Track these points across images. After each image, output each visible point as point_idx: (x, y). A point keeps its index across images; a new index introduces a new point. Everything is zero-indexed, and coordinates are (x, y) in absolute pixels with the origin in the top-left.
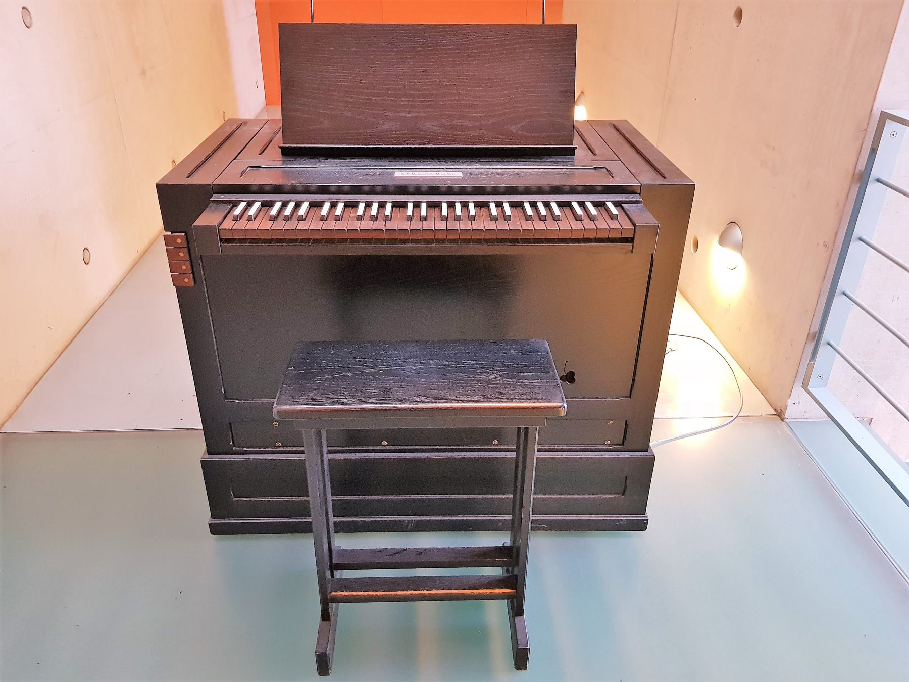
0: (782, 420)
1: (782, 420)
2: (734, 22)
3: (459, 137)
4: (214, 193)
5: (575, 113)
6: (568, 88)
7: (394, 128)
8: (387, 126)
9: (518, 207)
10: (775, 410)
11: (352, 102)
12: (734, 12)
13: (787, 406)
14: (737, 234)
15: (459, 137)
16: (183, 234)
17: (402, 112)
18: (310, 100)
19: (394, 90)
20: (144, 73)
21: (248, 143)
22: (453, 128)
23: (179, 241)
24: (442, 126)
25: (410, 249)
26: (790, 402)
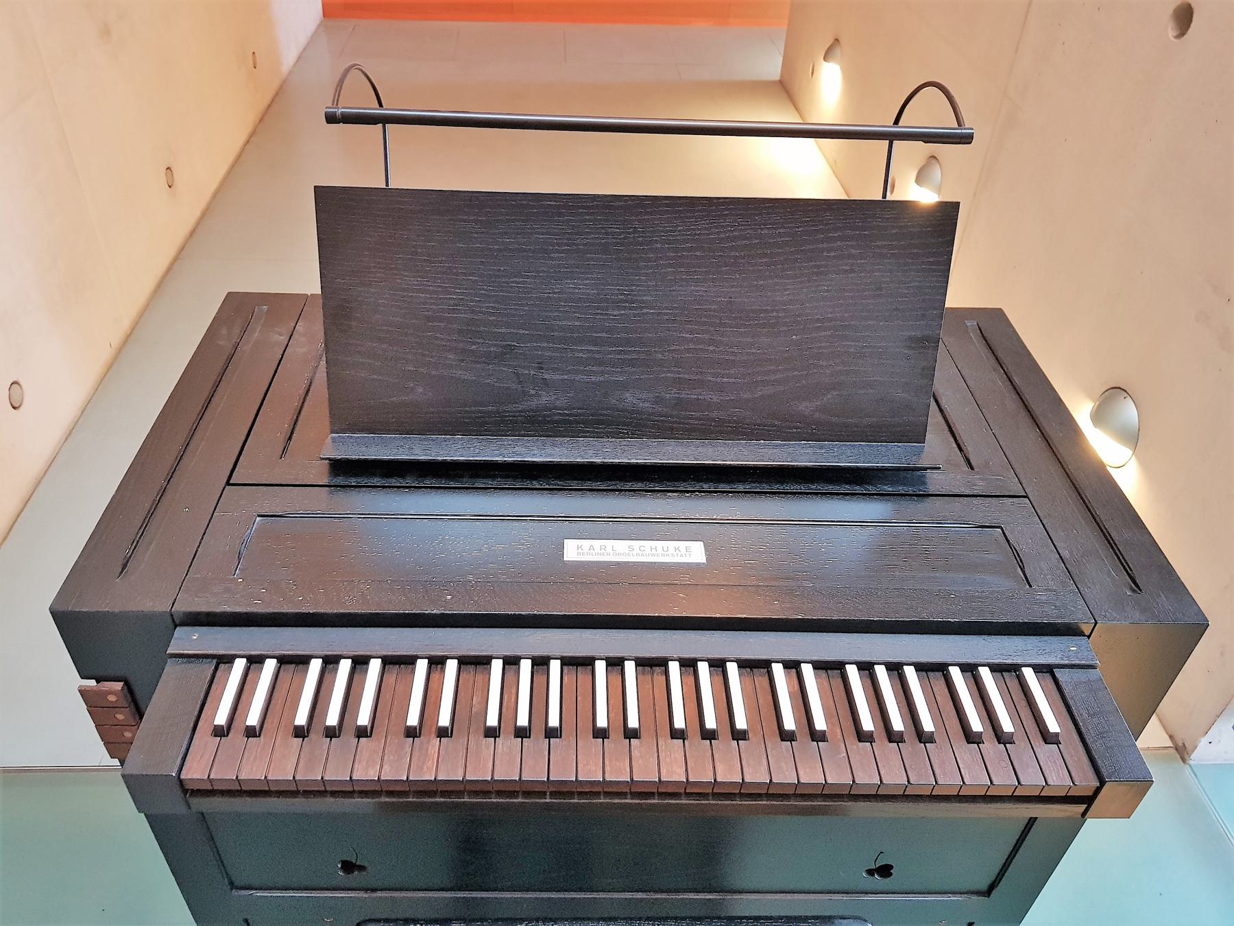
0: (1184, 760)
1: (1184, 760)
2: (1170, 29)
3: (691, 421)
4: (176, 626)
5: (1047, 722)
6: (926, 333)
7: (558, 403)
8: (545, 399)
9: (831, 669)
10: (1171, 737)
11: (472, 351)
12: (1174, 8)
13: (1196, 747)
14: (1129, 412)
15: (691, 421)
16: (118, 686)
17: (577, 372)
18: (385, 346)
19: (562, 329)
20: (106, 32)
21: (266, 394)
22: (679, 403)
23: (112, 698)
24: (658, 400)
25: (575, 484)
26: (1204, 742)
